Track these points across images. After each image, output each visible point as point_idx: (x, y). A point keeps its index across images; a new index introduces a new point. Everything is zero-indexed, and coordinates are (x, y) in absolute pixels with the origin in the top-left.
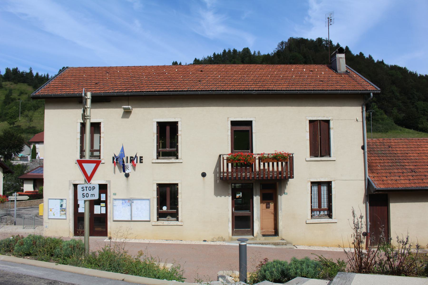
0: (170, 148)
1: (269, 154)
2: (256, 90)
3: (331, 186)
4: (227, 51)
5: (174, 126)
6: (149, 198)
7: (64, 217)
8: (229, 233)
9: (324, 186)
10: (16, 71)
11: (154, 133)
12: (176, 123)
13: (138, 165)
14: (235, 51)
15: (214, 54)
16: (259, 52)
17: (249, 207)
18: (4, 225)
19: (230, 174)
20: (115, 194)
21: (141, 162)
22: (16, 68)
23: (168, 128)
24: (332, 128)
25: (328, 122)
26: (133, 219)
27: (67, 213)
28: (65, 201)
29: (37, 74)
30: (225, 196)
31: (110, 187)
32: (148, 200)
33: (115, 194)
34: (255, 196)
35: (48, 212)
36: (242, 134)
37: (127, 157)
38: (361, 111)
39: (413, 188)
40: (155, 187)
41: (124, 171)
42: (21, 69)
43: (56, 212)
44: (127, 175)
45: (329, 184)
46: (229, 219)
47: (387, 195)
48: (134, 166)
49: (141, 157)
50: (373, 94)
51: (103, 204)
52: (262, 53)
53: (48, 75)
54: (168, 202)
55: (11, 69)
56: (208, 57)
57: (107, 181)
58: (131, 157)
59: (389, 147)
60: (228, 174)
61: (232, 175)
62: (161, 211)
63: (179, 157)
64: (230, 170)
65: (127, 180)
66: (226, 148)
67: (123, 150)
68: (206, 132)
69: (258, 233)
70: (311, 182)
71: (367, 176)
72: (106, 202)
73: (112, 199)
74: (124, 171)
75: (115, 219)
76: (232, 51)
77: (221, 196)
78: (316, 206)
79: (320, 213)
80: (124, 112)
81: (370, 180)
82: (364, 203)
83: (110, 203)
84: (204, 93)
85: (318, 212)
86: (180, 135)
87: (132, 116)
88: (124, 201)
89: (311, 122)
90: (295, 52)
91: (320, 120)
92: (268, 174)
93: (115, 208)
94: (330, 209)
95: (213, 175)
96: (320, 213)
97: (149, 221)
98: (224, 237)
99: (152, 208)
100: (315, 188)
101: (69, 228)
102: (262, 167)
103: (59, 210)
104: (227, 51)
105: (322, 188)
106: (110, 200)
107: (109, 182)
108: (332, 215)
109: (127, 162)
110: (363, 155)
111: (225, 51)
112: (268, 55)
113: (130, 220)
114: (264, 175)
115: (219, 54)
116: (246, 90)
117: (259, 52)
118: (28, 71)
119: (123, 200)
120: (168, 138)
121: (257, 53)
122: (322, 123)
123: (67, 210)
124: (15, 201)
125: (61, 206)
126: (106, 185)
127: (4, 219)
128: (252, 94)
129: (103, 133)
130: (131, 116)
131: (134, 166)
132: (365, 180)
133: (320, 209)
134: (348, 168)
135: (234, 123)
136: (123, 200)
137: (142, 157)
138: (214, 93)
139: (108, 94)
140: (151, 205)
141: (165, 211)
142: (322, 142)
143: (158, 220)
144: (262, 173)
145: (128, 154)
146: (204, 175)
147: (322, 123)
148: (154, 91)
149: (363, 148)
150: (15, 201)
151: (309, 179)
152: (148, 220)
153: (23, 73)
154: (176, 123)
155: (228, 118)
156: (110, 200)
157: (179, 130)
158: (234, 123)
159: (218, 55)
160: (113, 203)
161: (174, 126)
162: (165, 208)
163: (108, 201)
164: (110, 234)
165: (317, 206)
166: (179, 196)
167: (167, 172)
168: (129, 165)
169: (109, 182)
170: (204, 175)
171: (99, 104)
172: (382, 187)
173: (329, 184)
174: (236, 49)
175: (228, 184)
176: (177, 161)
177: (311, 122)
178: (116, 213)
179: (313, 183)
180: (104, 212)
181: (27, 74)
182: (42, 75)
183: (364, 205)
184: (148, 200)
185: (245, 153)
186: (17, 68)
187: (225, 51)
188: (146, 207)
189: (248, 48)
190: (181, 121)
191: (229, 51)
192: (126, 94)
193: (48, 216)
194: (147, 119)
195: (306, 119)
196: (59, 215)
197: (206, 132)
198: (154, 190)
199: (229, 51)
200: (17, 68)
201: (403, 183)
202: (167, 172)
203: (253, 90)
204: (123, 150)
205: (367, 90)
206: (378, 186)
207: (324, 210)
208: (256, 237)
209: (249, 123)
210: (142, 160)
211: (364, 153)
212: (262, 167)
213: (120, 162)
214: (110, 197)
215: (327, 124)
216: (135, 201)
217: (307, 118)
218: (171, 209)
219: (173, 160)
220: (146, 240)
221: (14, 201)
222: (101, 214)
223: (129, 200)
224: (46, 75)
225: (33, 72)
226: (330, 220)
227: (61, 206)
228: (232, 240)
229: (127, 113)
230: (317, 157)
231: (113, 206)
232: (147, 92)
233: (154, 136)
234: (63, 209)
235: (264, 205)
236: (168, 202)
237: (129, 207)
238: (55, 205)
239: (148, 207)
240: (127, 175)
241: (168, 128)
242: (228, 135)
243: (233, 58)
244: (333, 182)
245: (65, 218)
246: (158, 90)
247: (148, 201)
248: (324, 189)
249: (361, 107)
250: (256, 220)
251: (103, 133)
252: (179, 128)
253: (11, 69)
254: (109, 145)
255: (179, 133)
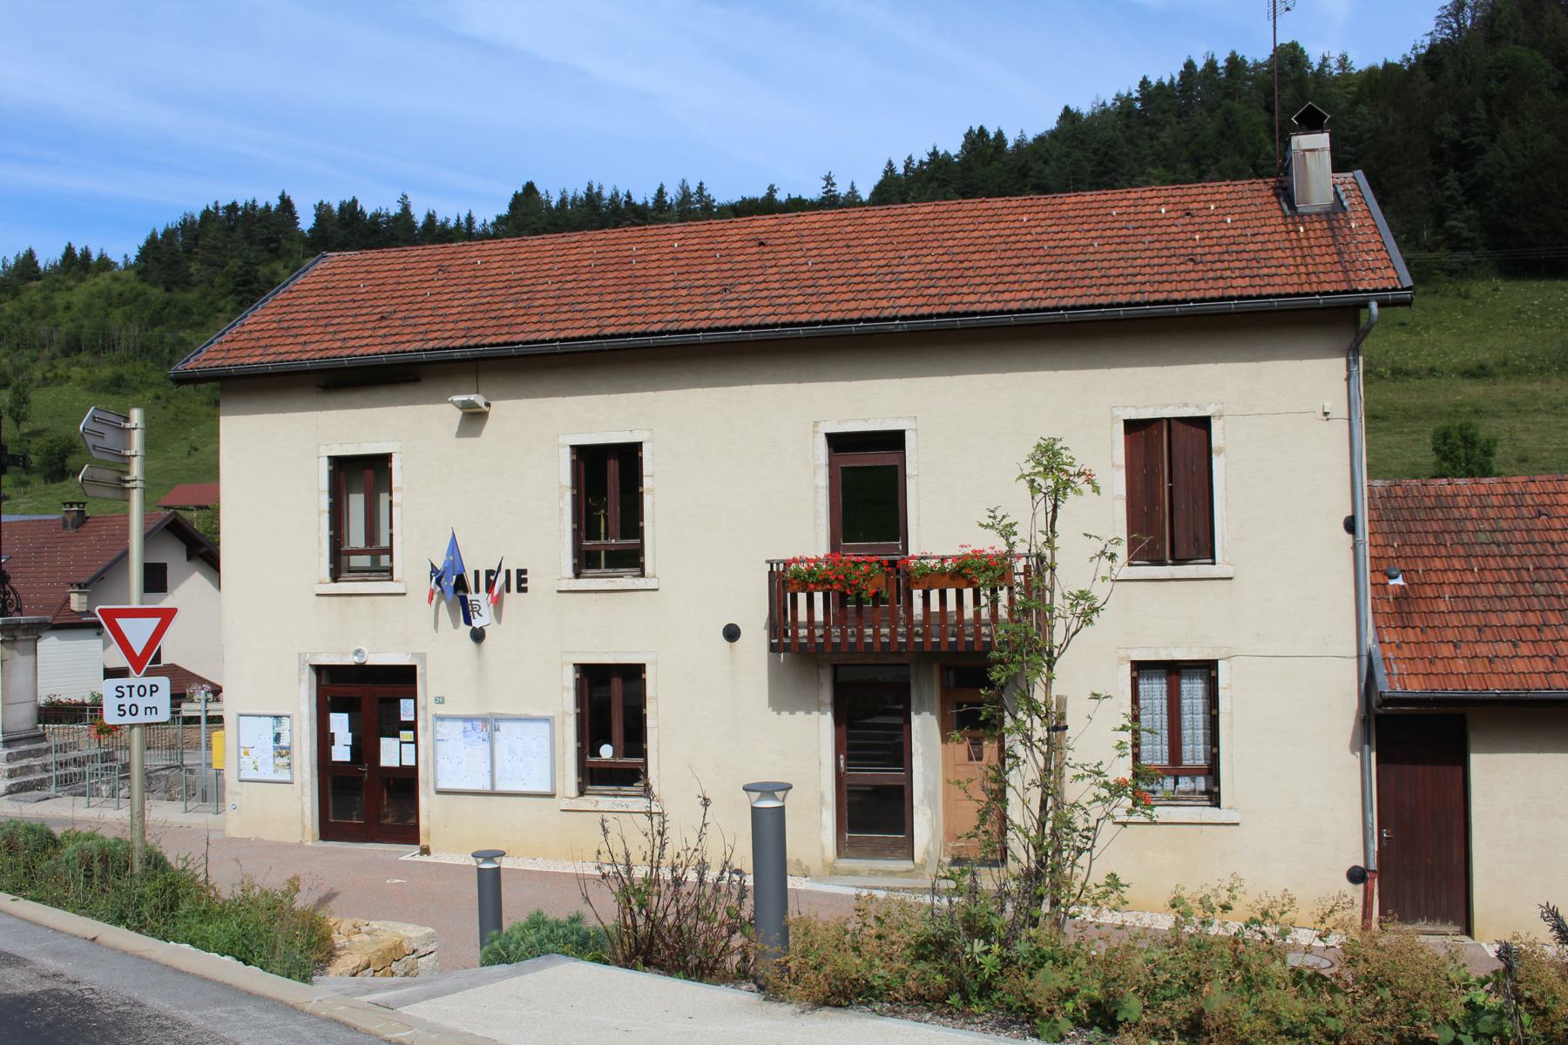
0: (622, 538)
1: (943, 559)
2: (904, 318)
3: (1216, 678)
4: (1200, 65)
5: (629, 455)
6: (549, 714)
7: (284, 775)
8: (823, 847)
9: (1191, 677)
10: (350, 210)
11: (561, 487)
12: (637, 447)
13: (512, 599)
14: (1235, 63)
15: (1144, 83)
16: (1343, 61)
17: (899, 755)
18: (161, 799)
19: (818, 632)
20: (440, 701)
21: (522, 590)
22: (349, 199)
23: (613, 467)
24: (1220, 451)
25: (1204, 423)
26: (500, 787)
27: (296, 765)
28: (286, 721)
29: (431, 218)
30: (808, 712)
31: (425, 674)
32: (546, 720)
33: (440, 701)
34: (918, 713)
35: (239, 757)
36: (868, 480)
37: (477, 573)
38: (1344, 373)
39: (1554, 694)
40: (569, 678)
41: (468, 621)
42: (369, 207)
43: (261, 761)
44: (478, 636)
45: (1207, 669)
46: (822, 797)
47: (1463, 718)
48: (498, 602)
49: (521, 572)
50: (1380, 306)
51: (406, 735)
52: (1359, 64)
53: (470, 219)
54: (617, 730)
55: (336, 207)
56: (1118, 97)
57: (413, 655)
58: (489, 573)
59: (1540, 514)
60: (811, 633)
61: (827, 635)
62: (595, 760)
63: (647, 571)
64: (819, 616)
65: (479, 652)
66: (808, 535)
67: (454, 546)
68: (740, 473)
69: (927, 852)
70: (1133, 662)
71: (1370, 639)
72: (412, 726)
73: (430, 718)
74: (468, 621)
75: (442, 785)
76: (1221, 63)
77: (792, 713)
78: (1156, 752)
79: (1176, 783)
80: (465, 414)
81: (1377, 657)
82: (1353, 752)
83: (426, 730)
84: (719, 336)
85: (1169, 782)
86: (651, 490)
87: (490, 425)
88: (469, 725)
89: (1131, 426)
90: (1516, 42)
91: (1169, 419)
92: (960, 634)
93: (441, 746)
94: (1212, 770)
95: (763, 635)
96: (1176, 783)
97: (552, 796)
98: (805, 862)
99: (558, 750)
100: (1155, 689)
101: (303, 813)
102: (935, 606)
103: (271, 752)
104: (1200, 65)
105: (1186, 686)
106: (426, 721)
107: (423, 657)
108: (1218, 795)
109: (477, 590)
110: (1351, 553)
111: (1190, 65)
112: (1388, 66)
113: (488, 788)
114: (943, 634)
115: (1166, 81)
116: (869, 320)
117: (1343, 61)
118: (395, 210)
119: (466, 719)
120: (608, 496)
121: (1333, 64)
122: (1180, 429)
123: (295, 750)
124: (203, 720)
125: (277, 738)
126: (413, 669)
127: (157, 778)
128: (890, 333)
129: (400, 489)
130: (485, 431)
131: (498, 602)
132: (1359, 656)
133: (1175, 765)
134: (1289, 606)
135: (839, 443)
136: (466, 719)
137: (524, 572)
138: (751, 335)
139: (411, 357)
140: (558, 738)
141: (607, 762)
142: (1181, 506)
143: (582, 793)
144: (935, 630)
145: (475, 562)
146: (732, 633)
147: (1177, 427)
148: (551, 341)
149: (1350, 525)
150: (203, 720)
151: (1122, 653)
152: (547, 789)
153: (377, 216)
154: (637, 447)
155: (816, 423)
156: (426, 721)
157: (645, 472)
158: (839, 443)
159: (1160, 85)
160: (435, 731)
161: (629, 455)
162: (606, 751)
163: (420, 725)
164: (428, 835)
165: (1166, 755)
166: (650, 710)
167: (609, 623)
168: (480, 599)
169: (423, 657)
170: (732, 633)
171: (341, 397)
172: (1415, 687)
173: (1207, 669)
174: (1239, 54)
175: (819, 666)
176: (640, 583)
177: (1131, 426)
178: (444, 764)
179: (1141, 669)
180: (409, 761)
181: (397, 218)
182: (448, 220)
183: (1355, 760)
184: (546, 720)
185: (879, 551)
186: (355, 201)
187: (1190, 65)
188: (543, 749)
189: (1294, 46)
190: (651, 440)
191: (1211, 65)
192: (457, 355)
193: (239, 770)
194: (542, 432)
195: (1114, 418)
196: (271, 768)
197: (740, 473)
198: (564, 688)
199: (1211, 65)
200: (355, 201)
201: (1521, 672)
202: (609, 623)
203: (895, 318)
204: (454, 546)
205: (1356, 291)
206: (1398, 682)
207: (1193, 773)
208: (923, 866)
209: (895, 440)
210: (525, 581)
211: (1355, 548)
212: (935, 606)
213: (455, 587)
214: (425, 708)
215: (1204, 432)
216: (503, 726)
217: (1117, 412)
218: (627, 755)
219: (627, 582)
220: (539, 860)
221: (197, 720)
222: (402, 769)
223: (485, 720)
224: (463, 220)
225: (413, 210)
226: (1210, 814)
227: (277, 738)
228: (834, 872)
229: (474, 418)
230: (1161, 563)
231: (436, 740)
232: (528, 342)
233: (562, 497)
234: (282, 751)
235: (962, 749)
236: (617, 730)
237: (486, 746)
238: (257, 735)
239: (547, 744)
240: (478, 636)
241: (613, 467)
242: (816, 488)
243: (1228, 95)
244: (1221, 664)
245: (288, 778)
246: (562, 335)
247: (546, 726)
248: (1193, 690)
249: (1343, 360)
250: (922, 802)
251: (400, 489)
252: (647, 468)
253: (336, 207)
254: (418, 527)
255: (647, 482)
